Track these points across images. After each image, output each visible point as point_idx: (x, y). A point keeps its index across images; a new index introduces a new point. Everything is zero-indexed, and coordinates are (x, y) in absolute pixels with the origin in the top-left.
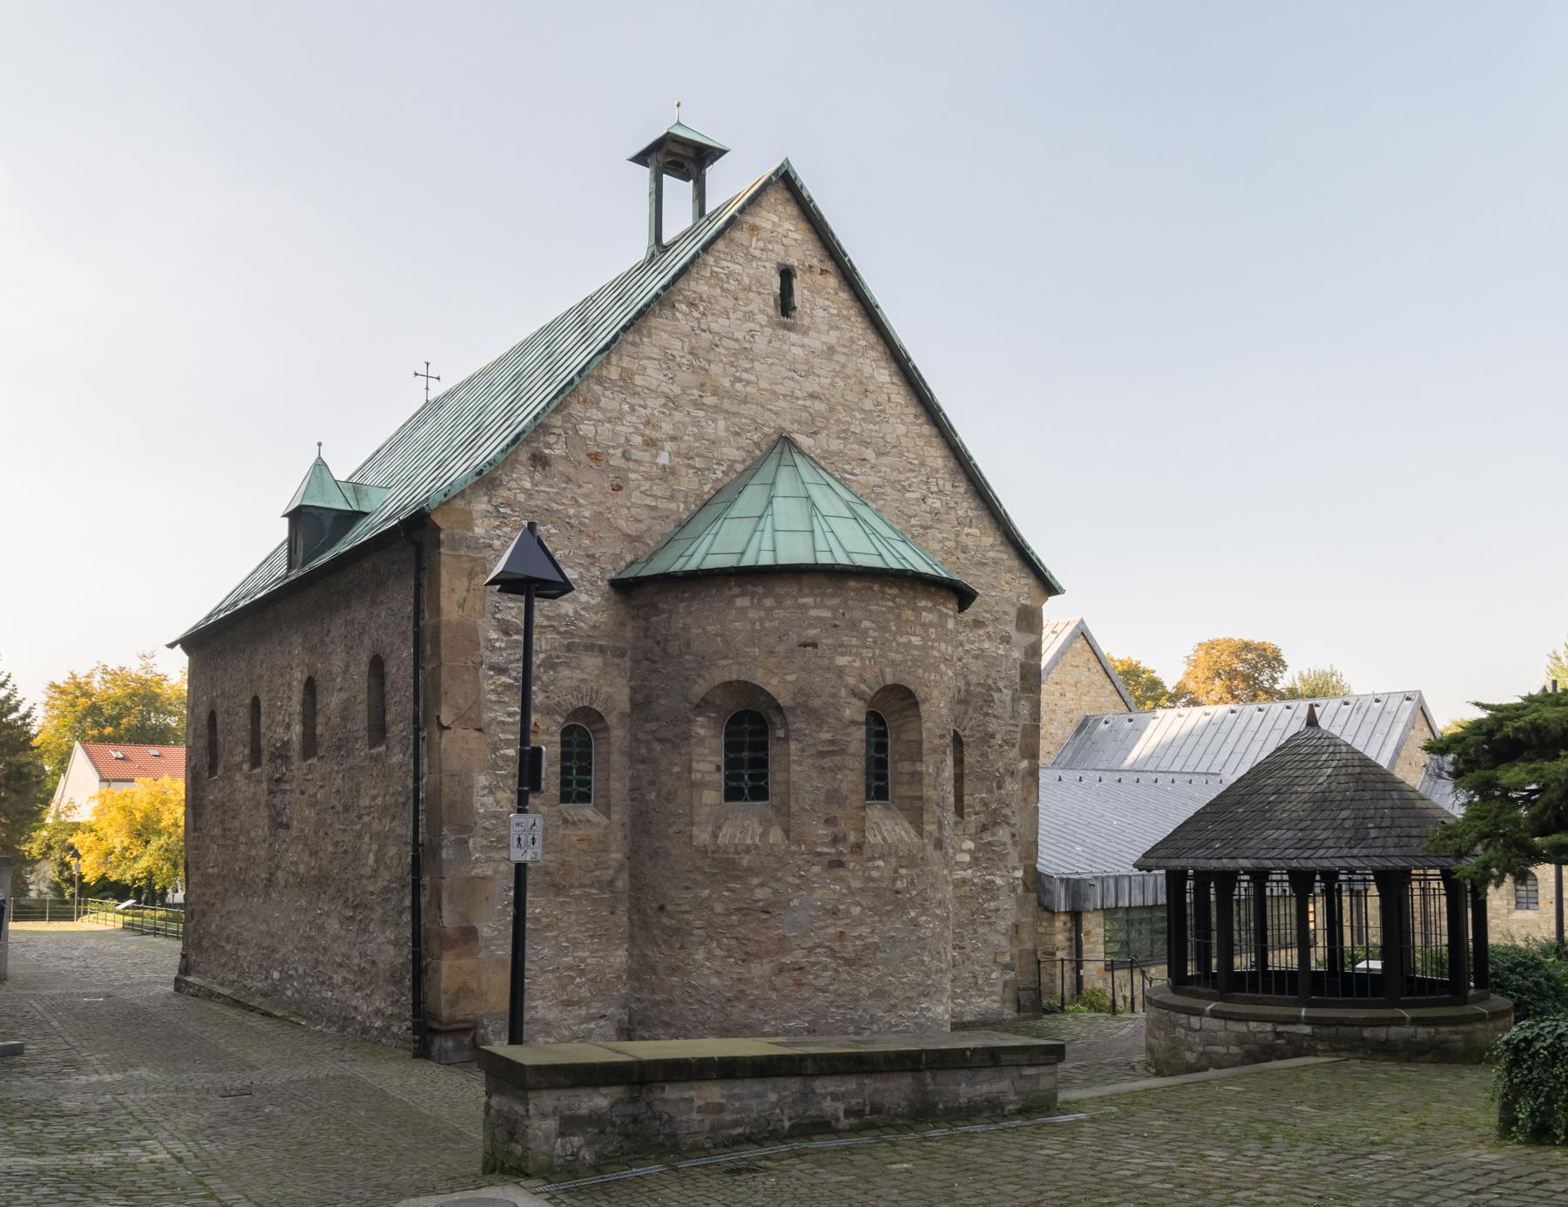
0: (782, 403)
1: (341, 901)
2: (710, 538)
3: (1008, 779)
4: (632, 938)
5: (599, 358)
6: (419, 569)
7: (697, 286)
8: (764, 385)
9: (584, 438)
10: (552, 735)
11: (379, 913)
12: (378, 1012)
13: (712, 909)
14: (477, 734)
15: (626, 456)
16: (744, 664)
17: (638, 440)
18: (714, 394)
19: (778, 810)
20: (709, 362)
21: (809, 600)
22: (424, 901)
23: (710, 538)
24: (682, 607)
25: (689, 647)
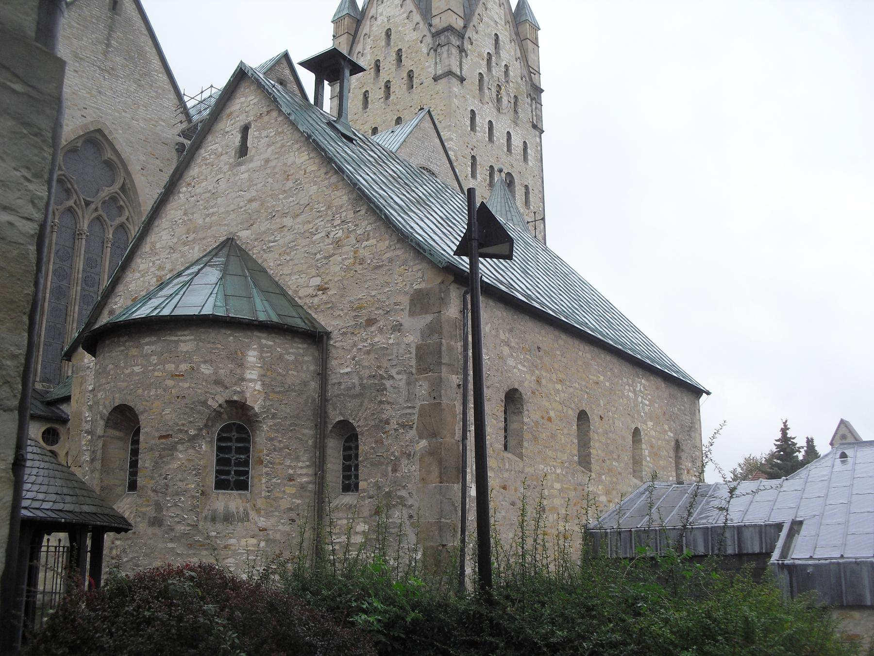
3: (404, 461)
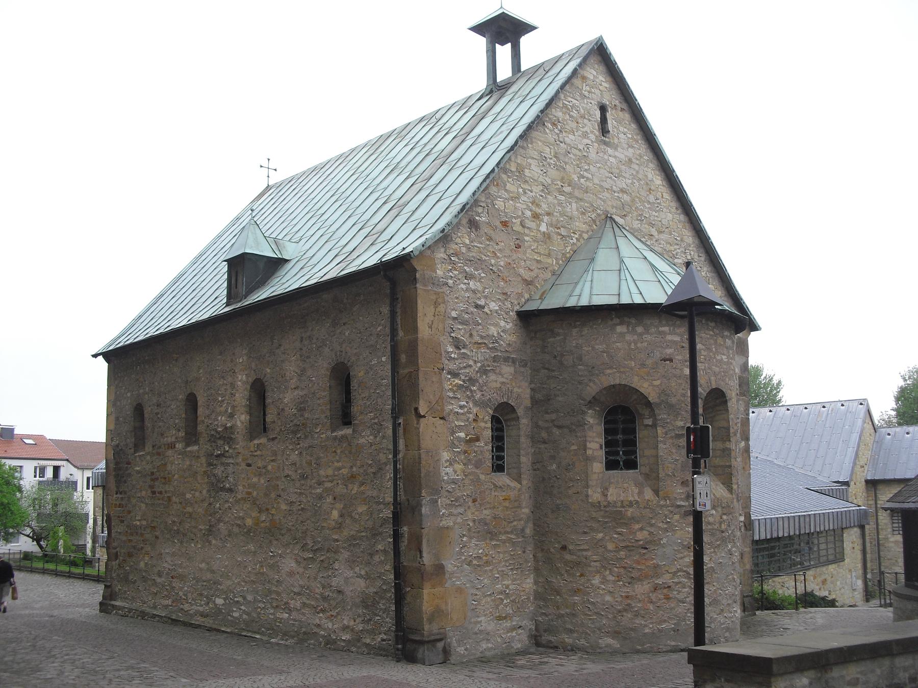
0: (607, 195)
1: (298, 546)
2: (588, 284)
4: (537, 570)
5: (508, 155)
6: (394, 300)
7: (557, 113)
8: (596, 181)
9: (498, 210)
10: (486, 422)
11: (345, 554)
12: (345, 628)
13: (605, 548)
14: (442, 421)
15: (522, 225)
16: (624, 372)
17: (528, 213)
18: (569, 186)
19: (647, 476)
20: (566, 163)
21: (666, 329)
22: (404, 545)
23: (588, 284)
24: (575, 331)
25: (581, 360)
